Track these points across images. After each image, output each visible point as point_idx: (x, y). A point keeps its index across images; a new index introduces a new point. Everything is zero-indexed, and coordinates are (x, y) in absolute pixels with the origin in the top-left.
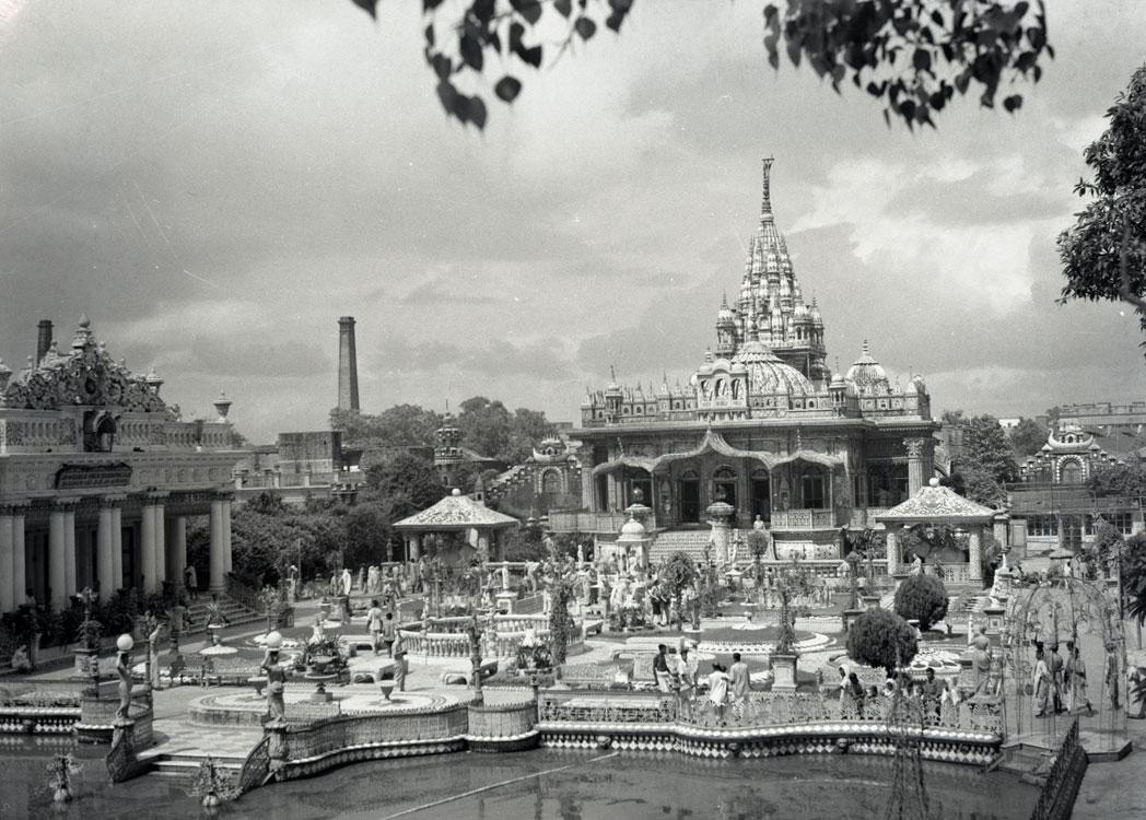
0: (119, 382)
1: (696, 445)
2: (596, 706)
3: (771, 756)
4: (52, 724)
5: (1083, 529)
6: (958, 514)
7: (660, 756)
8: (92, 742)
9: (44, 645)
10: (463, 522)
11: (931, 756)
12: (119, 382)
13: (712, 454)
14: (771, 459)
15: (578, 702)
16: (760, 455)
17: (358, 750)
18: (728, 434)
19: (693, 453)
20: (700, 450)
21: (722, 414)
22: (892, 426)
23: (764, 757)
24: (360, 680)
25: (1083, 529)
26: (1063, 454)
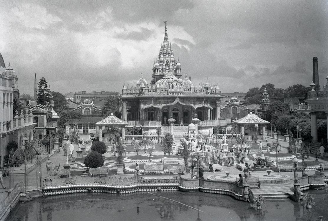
2: (156, 179)
3: (103, 192)
4: (169, 188)
5: (89, 128)
6: (105, 123)
7: (143, 193)
8: (317, 189)
11: (71, 192)
15: (146, 178)
16: (192, 105)
18: (181, 99)
19: (183, 104)
21: (176, 93)
23: (110, 193)
24: (216, 170)
25: (89, 128)
26: (85, 107)
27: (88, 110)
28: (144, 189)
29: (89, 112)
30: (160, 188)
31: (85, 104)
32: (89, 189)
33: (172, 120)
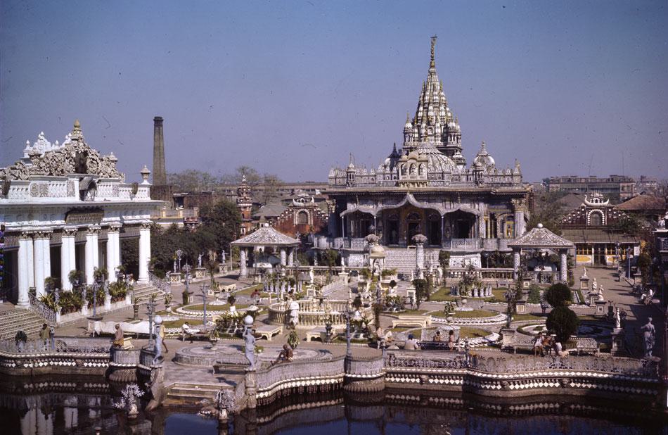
0: (96, 161)
1: (399, 202)
4: (492, 384)
9: (63, 313)
10: (272, 243)
12: (96, 161)
13: (408, 204)
14: (443, 208)
17: (289, 382)
18: (418, 195)
20: (403, 203)
22: (506, 192)
27: (598, 216)
28: (405, 378)
29: (598, 220)
30: (424, 377)
31: (592, 202)
32: (564, 380)
33: (422, 237)
